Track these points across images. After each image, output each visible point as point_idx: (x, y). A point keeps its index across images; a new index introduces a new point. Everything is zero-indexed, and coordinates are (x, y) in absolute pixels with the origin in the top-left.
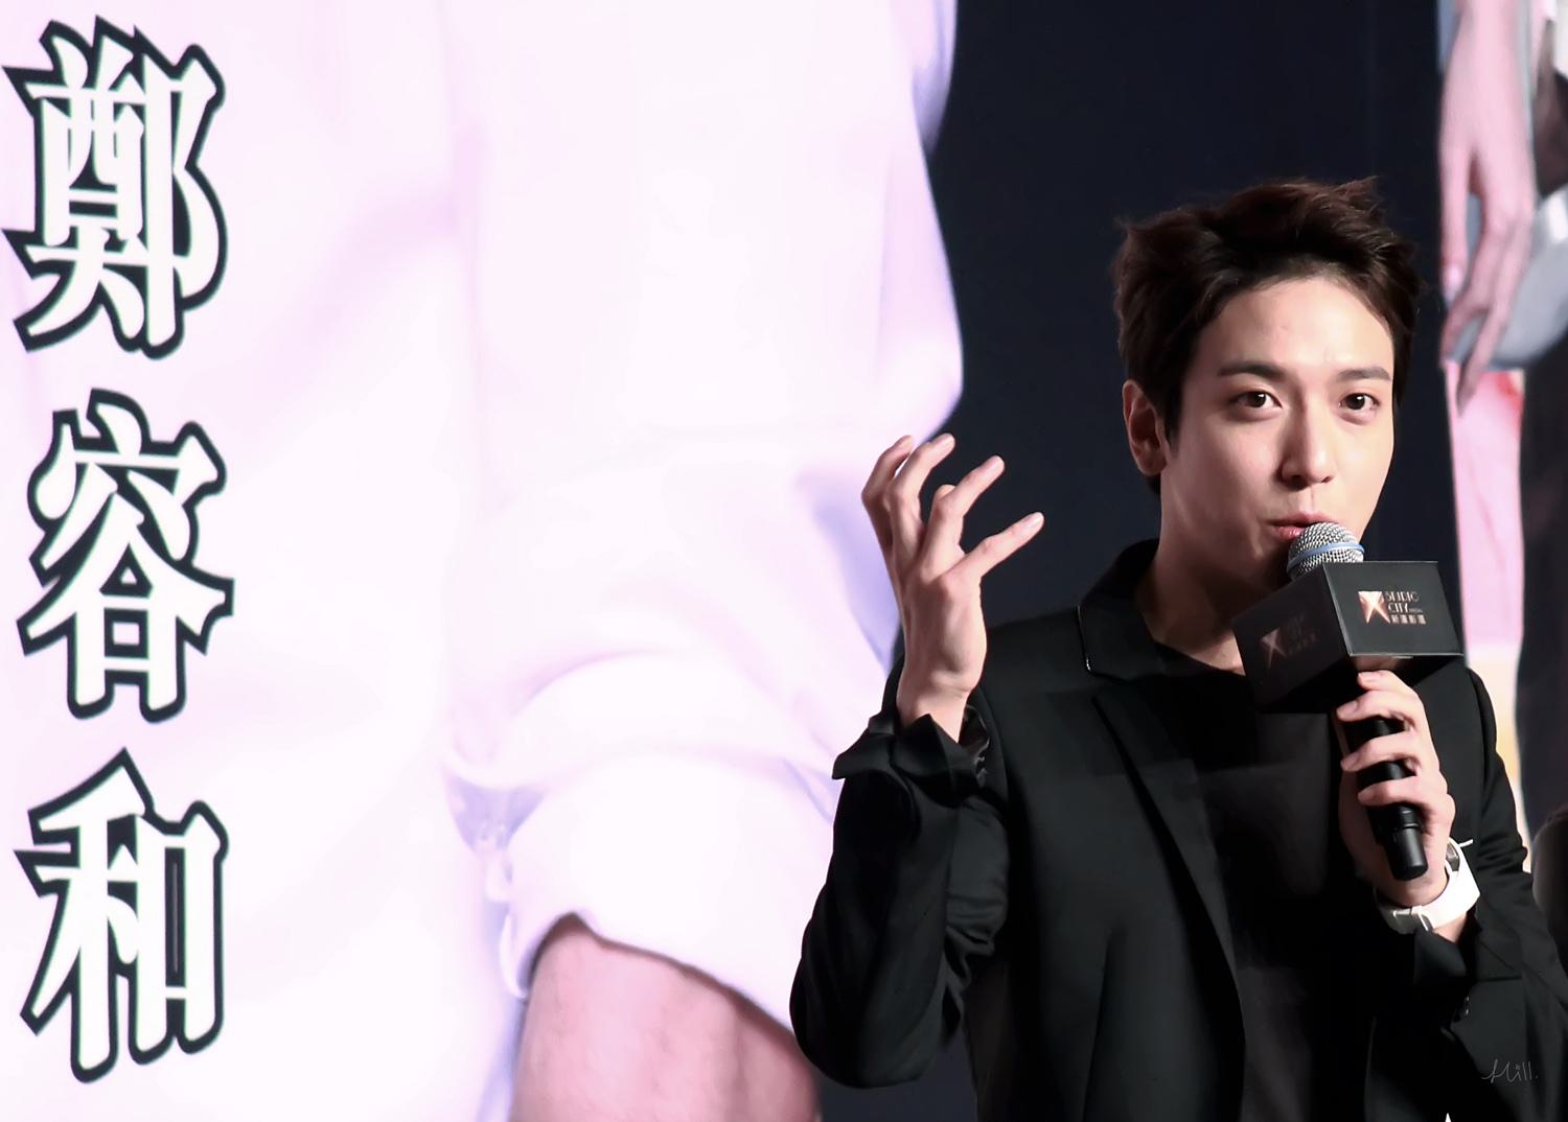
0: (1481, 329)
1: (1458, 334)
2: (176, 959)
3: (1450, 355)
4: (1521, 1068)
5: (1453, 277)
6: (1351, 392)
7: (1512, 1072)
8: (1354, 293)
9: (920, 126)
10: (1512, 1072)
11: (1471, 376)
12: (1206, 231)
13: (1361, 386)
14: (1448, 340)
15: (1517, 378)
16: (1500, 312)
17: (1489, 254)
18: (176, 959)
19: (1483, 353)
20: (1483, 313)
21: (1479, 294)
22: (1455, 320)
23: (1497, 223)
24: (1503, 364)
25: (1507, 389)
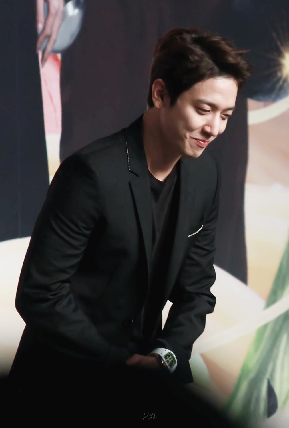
0: (49, 41)
1: (41, 43)
2: (63, 235)
3: (39, 49)
4: (152, 415)
5: (40, 26)
6: (200, 129)
7: (150, 416)
9: (236, 85)
10: (150, 416)
11: (46, 55)
14: (39, 45)
15: (59, 56)
16: (54, 37)
17: (50, 20)
18: (63, 235)
19: (49, 49)
20: (49, 37)
21: (48, 31)
22: (41, 39)
23: (52, 10)
24: (55, 52)
25: (56, 59)
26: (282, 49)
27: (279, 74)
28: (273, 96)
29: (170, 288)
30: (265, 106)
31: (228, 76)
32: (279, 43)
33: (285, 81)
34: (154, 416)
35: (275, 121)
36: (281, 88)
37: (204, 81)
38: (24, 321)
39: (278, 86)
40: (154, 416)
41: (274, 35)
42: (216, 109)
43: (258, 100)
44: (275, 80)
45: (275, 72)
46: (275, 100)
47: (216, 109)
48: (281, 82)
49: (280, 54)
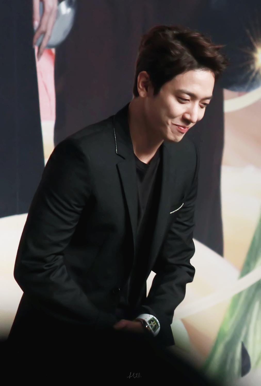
0: (44, 37)
1: (37, 39)
2: (57, 212)
3: (35, 44)
4: (137, 374)
5: (36, 23)
7: (135, 375)
8: (184, 73)
9: (213, 76)
10: (135, 375)
11: (41, 50)
14: (35, 40)
15: (53, 50)
16: (48, 33)
17: (45, 18)
18: (57, 212)
19: (44, 44)
20: (44, 33)
21: (43, 28)
22: (37, 35)
23: (47, 9)
24: (50, 47)
25: (51, 53)
26: (255, 44)
27: (252, 67)
28: (247, 87)
30: (240, 95)
31: (206, 69)
32: (252, 39)
33: (257, 73)
34: (139, 375)
35: (249, 109)
36: (254, 80)
38: (22, 289)
39: (251, 78)
40: (139, 375)
41: (248, 31)
42: (195, 98)
43: (233, 90)
44: (248, 72)
45: (249, 65)
46: (248, 90)
47: (195, 98)
48: (254, 74)
49: (253, 49)
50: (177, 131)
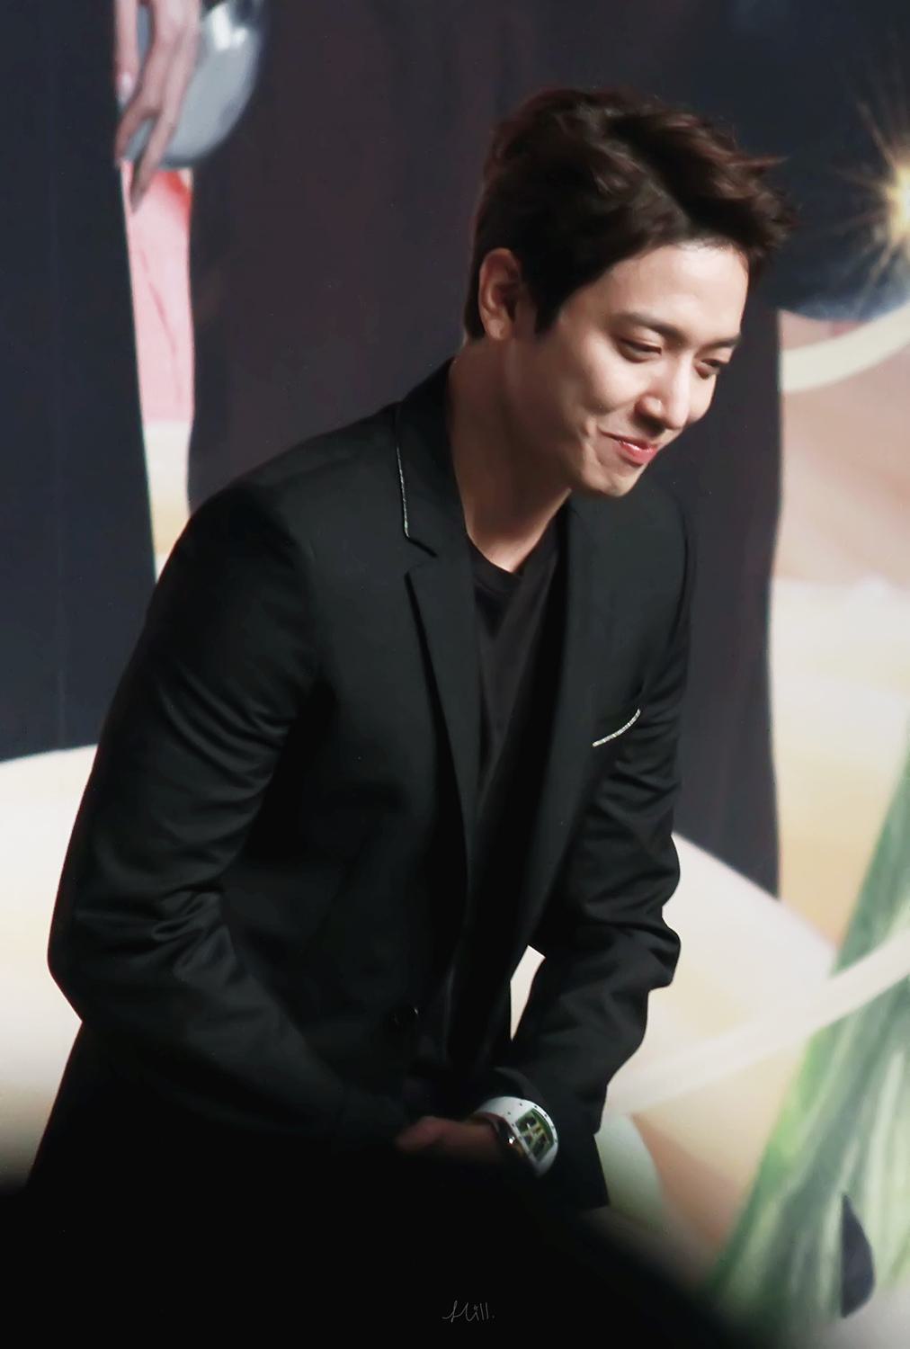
0: (153, 129)
1: (130, 136)
2: (198, 740)
3: (123, 154)
4: (479, 1308)
5: (126, 82)
7: (471, 1312)
9: (744, 267)
10: (471, 1312)
11: (144, 174)
12: (686, 128)
13: (659, 228)
14: (121, 140)
15: (186, 176)
16: (169, 116)
17: (159, 62)
18: (198, 740)
19: (155, 153)
20: (154, 116)
21: (150, 98)
22: (129, 122)
23: (165, 33)
24: (173, 163)
25: (176, 186)
26: (888, 154)
27: (878, 234)
28: (860, 303)
29: (536, 907)
30: (836, 333)
32: (878, 136)
33: (897, 255)
34: (485, 1312)
35: (867, 381)
36: (885, 278)
37: (643, 257)
39: (875, 272)
40: (485, 1312)
41: (864, 110)
42: (681, 343)
43: (814, 314)
44: (866, 251)
45: (867, 228)
46: (865, 315)
47: (681, 343)
48: (885, 260)
49: (883, 172)
50: (616, 459)
